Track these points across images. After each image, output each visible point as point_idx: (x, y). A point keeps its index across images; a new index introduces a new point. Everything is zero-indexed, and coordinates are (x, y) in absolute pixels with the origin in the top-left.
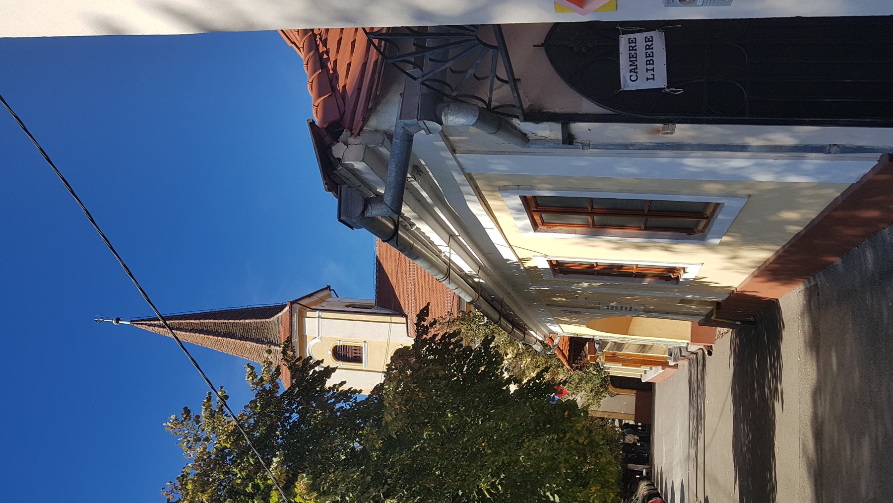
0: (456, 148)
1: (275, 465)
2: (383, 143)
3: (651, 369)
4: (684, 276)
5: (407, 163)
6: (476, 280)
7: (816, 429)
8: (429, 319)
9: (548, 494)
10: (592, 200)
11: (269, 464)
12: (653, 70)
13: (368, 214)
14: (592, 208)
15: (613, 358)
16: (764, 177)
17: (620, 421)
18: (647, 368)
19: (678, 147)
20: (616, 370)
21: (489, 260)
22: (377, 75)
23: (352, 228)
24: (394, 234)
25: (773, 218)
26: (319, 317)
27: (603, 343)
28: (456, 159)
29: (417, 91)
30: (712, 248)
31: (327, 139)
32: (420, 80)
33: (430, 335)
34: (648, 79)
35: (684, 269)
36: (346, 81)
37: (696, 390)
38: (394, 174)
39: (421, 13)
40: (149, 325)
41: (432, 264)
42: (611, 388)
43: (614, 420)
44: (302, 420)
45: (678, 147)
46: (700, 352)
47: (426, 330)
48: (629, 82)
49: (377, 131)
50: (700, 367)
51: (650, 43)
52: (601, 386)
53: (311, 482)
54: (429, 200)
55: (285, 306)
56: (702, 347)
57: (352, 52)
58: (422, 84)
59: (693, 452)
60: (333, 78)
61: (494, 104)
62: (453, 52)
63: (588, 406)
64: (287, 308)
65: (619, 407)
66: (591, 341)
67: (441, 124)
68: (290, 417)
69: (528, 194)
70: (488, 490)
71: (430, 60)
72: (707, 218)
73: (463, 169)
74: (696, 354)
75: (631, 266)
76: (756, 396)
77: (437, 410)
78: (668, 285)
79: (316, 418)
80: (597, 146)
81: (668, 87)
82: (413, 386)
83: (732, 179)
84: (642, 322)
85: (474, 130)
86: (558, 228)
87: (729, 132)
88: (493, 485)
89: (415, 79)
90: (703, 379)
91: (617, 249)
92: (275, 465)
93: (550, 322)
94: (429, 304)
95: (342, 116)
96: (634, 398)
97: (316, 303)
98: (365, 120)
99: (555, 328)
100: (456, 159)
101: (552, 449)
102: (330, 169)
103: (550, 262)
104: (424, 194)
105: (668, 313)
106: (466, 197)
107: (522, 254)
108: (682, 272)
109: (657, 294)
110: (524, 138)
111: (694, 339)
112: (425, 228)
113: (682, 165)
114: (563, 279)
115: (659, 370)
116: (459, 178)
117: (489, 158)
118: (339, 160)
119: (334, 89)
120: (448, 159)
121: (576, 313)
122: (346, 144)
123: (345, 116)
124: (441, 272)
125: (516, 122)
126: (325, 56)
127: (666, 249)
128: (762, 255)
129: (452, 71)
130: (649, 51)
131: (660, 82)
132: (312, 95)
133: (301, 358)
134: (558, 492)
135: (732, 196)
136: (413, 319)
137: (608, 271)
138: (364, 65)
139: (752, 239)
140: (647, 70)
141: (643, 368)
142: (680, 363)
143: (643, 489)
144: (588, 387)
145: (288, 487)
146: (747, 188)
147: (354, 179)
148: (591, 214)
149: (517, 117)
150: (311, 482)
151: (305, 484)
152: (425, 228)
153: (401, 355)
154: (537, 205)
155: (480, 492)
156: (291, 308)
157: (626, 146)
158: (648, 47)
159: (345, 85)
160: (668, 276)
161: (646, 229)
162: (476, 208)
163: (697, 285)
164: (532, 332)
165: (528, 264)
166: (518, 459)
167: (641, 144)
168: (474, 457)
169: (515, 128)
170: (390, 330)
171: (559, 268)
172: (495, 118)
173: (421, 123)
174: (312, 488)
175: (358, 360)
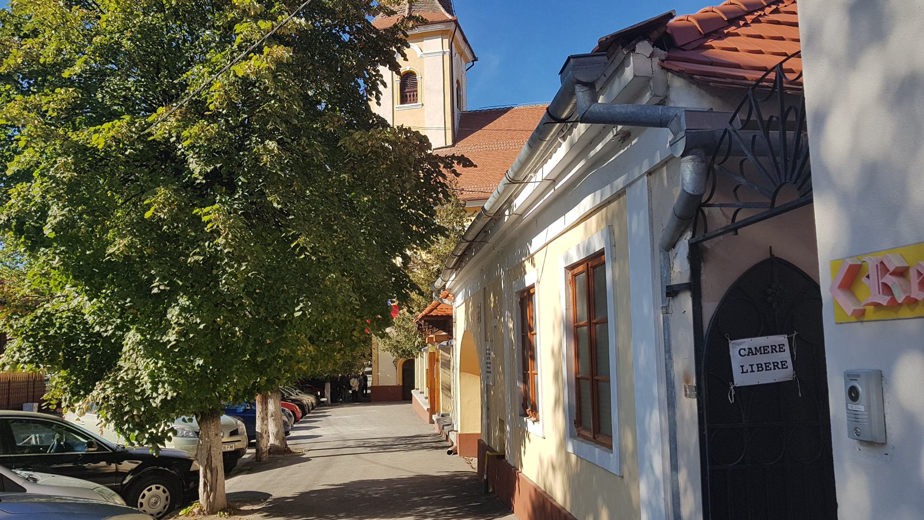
0: (653, 176)
1: (298, 21)
2: (655, 95)
3: (426, 398)
4: (529, 422)
5: (634, 123)
6: (507, 213)
8: (458, 168)
9: (301, 305)
10: (605, 321)
11: (298, 15)
12: (752, 371)
13: (578, 89)
14: (595, 324)
15: (433, 359)
16: (643, 490)
17: (370, 373)
18: (426, 394)
19: (671, 403)
20: (421, 365)
21: (529, 224)
22: (730, 80)
23: (561, 73)
24: (555, 118)
25: (600, 501)
26: (444, 53)
27: (448, 349)
28: (641, 176)
29: (717, 126)
30: (562, 446)
31: (655, 35)
32: (730, 128)
33: (444, 171)
34: (742, 367)
35: (537, 420)
36: (717, 48)
37: (411, 443)
38: (624, 111)
39: (821, 118)
41: (523, 164)
42: (401, 361)
43: (370, 366)
44: (344, 45)
45: (671, 403)
46: (449, 444)
47: (449, 166)
48: (737, 348)
49: (668, 87)
50: (434, 445)
51: (780, 366)
52: (403, 351)
53: (285, 61)
54: (592, 153)
55: (452, 15)
56: (455, 444)
57: (751, 52)
58: (726, 131)
59: (351, 443)
60: (719, 34)
61: (706, 210)
62: (765, 160)
64: (450, 17)
65: (385, 371)
66: (450, 336)
67: (683, 156)
68: (344, 32)
69: (607, 257)
70: (297, 245)
71: (754, 137)
72: (595, 438)
73: (629, 185)
74: (447, 440)
75: (535, 367)
76: (415, 499)
77: (370, 185)
78: (518, 408)
79: (348, 59)
80: (666, 321)
81: (735, 388)
82: (392, 157)
83: (639, 456)
84: (475, 386)
85: (677, 192)
86: (571, 291)
87: (692, 452)
88: (303, 249)
89: (731, 122)
90: (424, 448)
91: (553, 352)
92: (298, 21)
93: (466, 293)
94: (476, 166)
95: (681, 48)
96: (395, 384)
97: (458, 47)
98: (679, 74)
99: (460, 299)
100: (641, 176)
101: (345, 304)
102: (623, 41)
103: (533, 286)
104: (599, 147)
105: (488, 409)
106: (598, 192)
107: (538, 258)
108: (533, 419)
109: (508, 398)
110: (671, 245)
111: (462, 437)
112: (562, 152)
113: (652, 408)
114: (516, 300)
115: (427, 406)
116: (619, 183)
117: (644, 213)
118: (634, 50)
119: (708, 36)
120: (641, 168)
121: (479, 318)
122: (652, 56)
123: (682, 52)
124: (517, 174)
125: (688, 235)
126: (742, 23)
127: (557, 401)
128: (559, 494)
129: (742, 162)
130: (772, 366)
131: (740, 380)
132: (699, 13)
133: (407, 36)
134: (304, 314)
135: (621, 460)
136: (458, 151)
137: (527, 345)
138: (738, 66)
139: (575, 483)
140: (752, 365)
141: (426, 390)
142: (436, 425)
143: (308, 399)
144: (401, 338)
145: (277, 38)
146: (630, 473)
147: (613, 68)
148: (590, 324)
149: (693, 236)
150: (285, 61)
151: (282, 57)
152: (562, 152)
153: (424, 142)
154: (594, 267)
155: (295, 237)
156: (451, 21)
157: (668, 350)
158: (776, 365)
159: (713, 48)
160: (528, 406)
161: (578, 379)
162: (587, 204)
163: (521, 435)
164: (454, 276)
165: (528, 265)
166: (331, 272)
167: (672, 366)
168: (328, 227)
169: (681, 235)
170: (438, 128)
171: (526, 297)
172: (692, 213)
173: (683, 133)
174: (279, 63)
175: (404, 100)
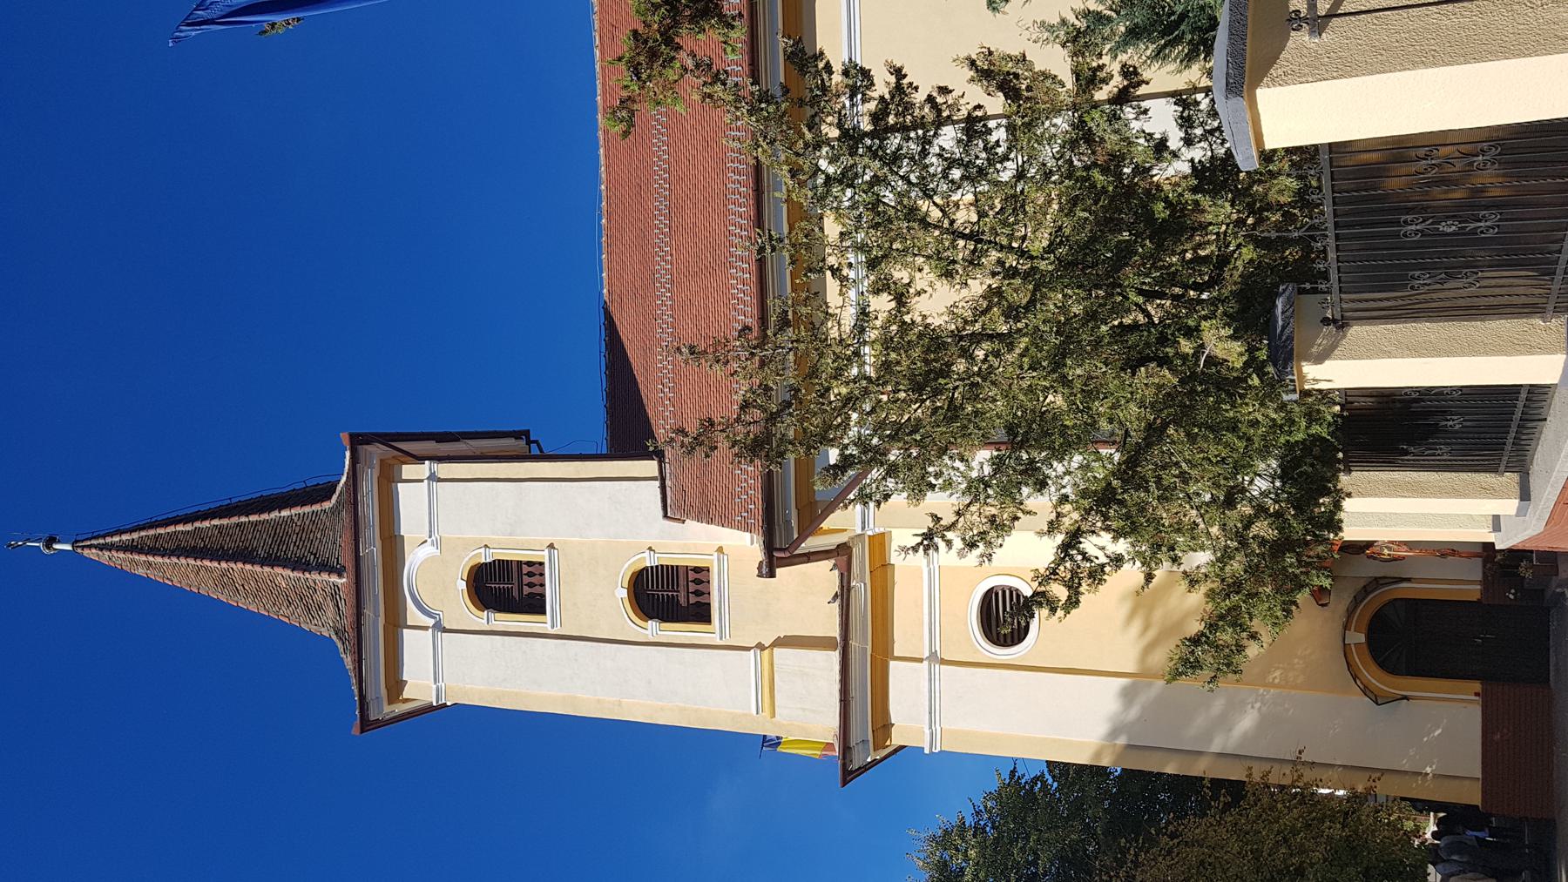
7: (1441, 393)
26: (433, 477)
40: (101, 548)
63: (915, 549)
175: (536, 605)
